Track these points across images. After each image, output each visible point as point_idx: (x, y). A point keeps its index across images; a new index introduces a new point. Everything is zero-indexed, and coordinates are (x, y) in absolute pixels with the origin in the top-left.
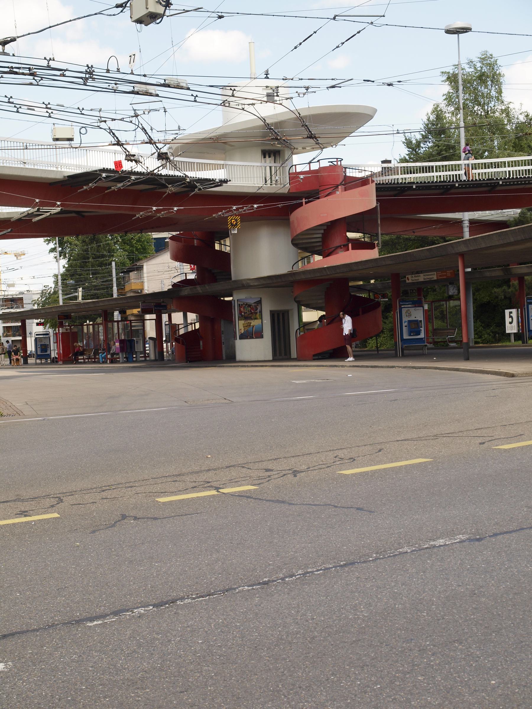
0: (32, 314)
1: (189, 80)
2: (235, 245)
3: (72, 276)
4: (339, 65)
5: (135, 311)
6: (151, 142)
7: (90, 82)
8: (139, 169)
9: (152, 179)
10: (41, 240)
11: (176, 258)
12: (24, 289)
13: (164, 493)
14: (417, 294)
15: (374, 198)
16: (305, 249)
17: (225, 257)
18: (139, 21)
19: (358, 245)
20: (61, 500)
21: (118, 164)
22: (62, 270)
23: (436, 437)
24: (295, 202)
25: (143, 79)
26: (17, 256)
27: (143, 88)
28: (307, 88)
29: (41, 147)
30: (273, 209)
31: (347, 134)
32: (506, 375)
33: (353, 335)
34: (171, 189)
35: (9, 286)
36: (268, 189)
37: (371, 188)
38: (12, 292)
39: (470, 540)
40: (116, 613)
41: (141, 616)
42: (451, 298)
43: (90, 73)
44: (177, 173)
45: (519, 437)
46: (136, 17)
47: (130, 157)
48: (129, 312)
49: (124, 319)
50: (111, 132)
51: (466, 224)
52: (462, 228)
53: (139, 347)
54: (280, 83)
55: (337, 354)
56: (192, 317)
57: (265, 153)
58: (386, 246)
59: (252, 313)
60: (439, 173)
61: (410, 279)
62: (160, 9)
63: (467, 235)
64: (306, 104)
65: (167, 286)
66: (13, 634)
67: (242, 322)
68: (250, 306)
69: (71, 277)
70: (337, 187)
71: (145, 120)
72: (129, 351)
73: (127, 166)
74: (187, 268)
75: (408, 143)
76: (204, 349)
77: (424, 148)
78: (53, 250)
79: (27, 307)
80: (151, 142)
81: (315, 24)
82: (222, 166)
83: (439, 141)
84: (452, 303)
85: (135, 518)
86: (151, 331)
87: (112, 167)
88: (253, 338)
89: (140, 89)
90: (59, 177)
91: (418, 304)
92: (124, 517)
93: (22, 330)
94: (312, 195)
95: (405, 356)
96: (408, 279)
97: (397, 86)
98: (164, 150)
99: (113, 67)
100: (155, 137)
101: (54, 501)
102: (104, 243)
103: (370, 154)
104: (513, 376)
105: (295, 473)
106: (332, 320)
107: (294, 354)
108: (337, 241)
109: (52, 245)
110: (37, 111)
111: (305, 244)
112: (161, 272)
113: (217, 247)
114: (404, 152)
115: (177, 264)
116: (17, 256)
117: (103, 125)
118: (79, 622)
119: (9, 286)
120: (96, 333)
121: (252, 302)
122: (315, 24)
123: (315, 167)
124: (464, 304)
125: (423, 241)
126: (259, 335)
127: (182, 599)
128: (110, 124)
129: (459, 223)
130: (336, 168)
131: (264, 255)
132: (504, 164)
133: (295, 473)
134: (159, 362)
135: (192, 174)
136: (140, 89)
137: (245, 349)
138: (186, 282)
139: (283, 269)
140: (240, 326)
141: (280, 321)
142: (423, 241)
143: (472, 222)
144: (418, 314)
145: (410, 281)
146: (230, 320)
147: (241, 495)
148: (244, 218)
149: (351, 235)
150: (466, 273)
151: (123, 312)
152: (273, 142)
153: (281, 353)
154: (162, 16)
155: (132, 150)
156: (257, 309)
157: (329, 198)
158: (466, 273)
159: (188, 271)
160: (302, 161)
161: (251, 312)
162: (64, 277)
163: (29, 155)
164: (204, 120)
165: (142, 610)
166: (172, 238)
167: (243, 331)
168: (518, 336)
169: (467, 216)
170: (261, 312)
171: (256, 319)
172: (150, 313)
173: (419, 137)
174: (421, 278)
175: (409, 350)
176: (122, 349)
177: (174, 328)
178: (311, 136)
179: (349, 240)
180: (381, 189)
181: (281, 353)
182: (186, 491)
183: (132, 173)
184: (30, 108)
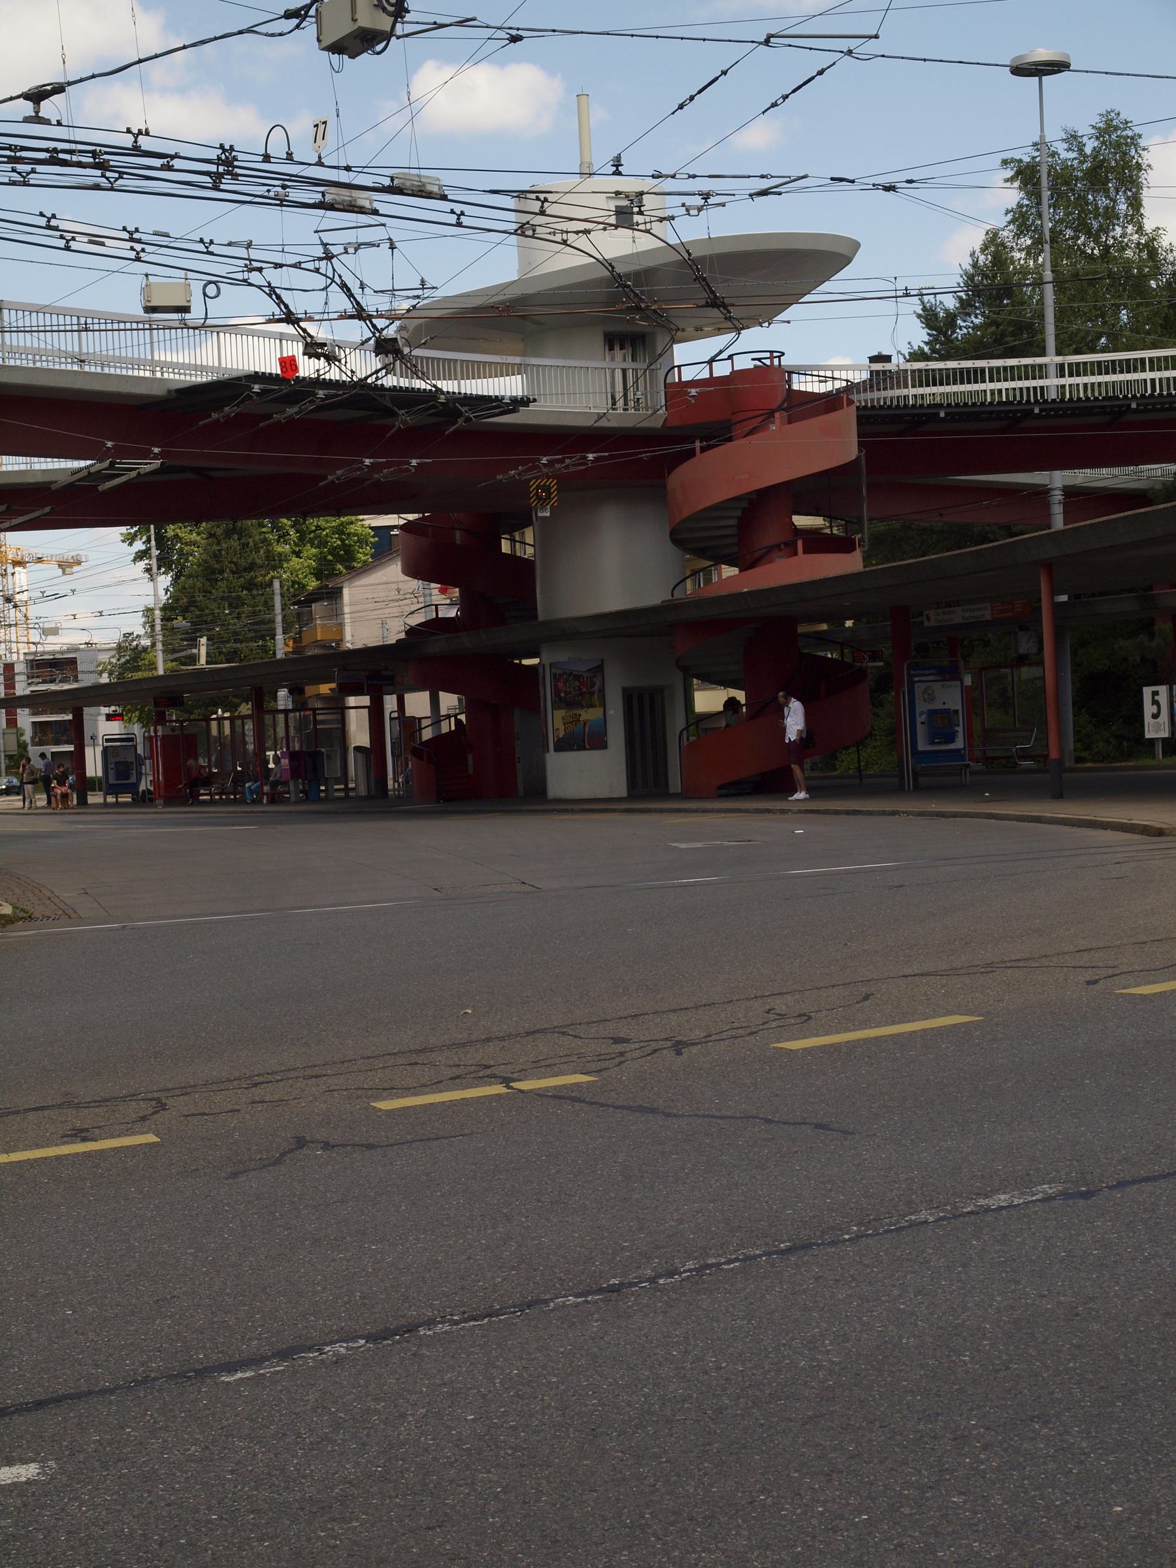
0: (98, 695)
1: (446, 178)
2: (543, 544)
3: (184, 611)
4: (760, 143)
5: (325, 689)
6: (360, 314)
7: (227, 183)
8: (334, 374)
9: (361, 394)
10: (115, 533)
11: (413, 570)
13: (390, 1091)
14: (948, 653)
16: (701, 553)
18: (337, 48)
19: (816, 542)
21: (288, 363)
22: (163, 598)
23: (990, 967)
24: (678, 448)
25: (344, 177)
26: (65, 565)
27: (344, 195)
28: (706, 196)
30: (629, 462)
31: (794, 298)
32: (1145, 830)
34: (404, 418)
35: (46, 632)
36: (622, 418)
37: (848, 418)
38: (53, 645)
40: (283, 1355)
41: (339, 1360)
42: (1022, 660)
43: (225, 164)
46: (329, 40)
47: (313, 349)
48: (310, 690)
49: (300, 703)
51: (1058, 496)
52: (1047, 506)
53: (331, 769)
54: (648, 184)
55: (771, 783)
56: (449, 701)
57: (613, 341)
58: (879, 547)
59: (582, 694)
60: (996, 383)
61: (934, 618)
63: (1058, 522)
64: (692, 230)
65: (394, 634)
66: (57, 1400)
67: (560, 714)
68: (577, 677)
69: (181, 614)
70: (771, 414)
71: (348, 267)
72: (310, 779)
73: (308, 368)
75: (929, 317)
76: (477, 774)
77: (964, 328)
78: (140, 556)
79: (86, 681)
80: (360, 314)
81: (724, 55)
84: (1026, 672)
85: (326, 1146)
86: (359, 732)
87: (276, 369)
88: (583, 748)
89: (340, 198)
91: (950, 673)
92: (301, 1143)
93: (76, 732)
94: (717, 433)
95: (920, 789)
96: (928, 618)
98: (391, 332)
99: (277, 149)
100: (371, 303)
101: (146, 1108)
103: (830, 343)
104: (1160, 833)
105: (678, 1047)
108: (771, 535)
109: (139, 545)
111: (698, 540)
112: (382, 604)
113: (505, 547)
114: (919, 336)
115: (415, 584)
116: (65, 565)
117: (255, 277)
118: (203, 1373)
119: (46, 632)
120: (238, 738)
121: (582, 668)
122: (724, 55)
123: (722, 369)
124: (1053, 673)
125: (963, 535)
126: (598, 741)
127: (430, 1323)
129: (1041, 494)
130: (769, 375)
131: (614, 567)
132: (1155, 364)
133: (678, 1047)
134: (376, 802)
135: (448, 386)
136: (340, 198)
137: (579, 773)
138: (436, 625)
139: (652, 595)
140: (556, 721)
141: (646, 713)
142: (963, 535)
143: (1070, 492)
144: (950, 697)
145: (933, 623)
147: (559, 1096)
148: (566, 483)
149: (800, 521)
151: (296, 691)
152: (630, 311)
153: (647, 784)
154: (387, 36)
155: (318, 331)
156: (593, 686)
157: (754, 439)
159: (444, 603)
160: (694, 357)
161: (581, 690)
163: (92, 344)
164: (480, 265)
166: (407, 527)
167: (562, 734)
169: (1059, 479)
170: (602, 691)
171: (592, 706)
172: (358, 692)
173: (950, 303)
174: (958, 616)
176: (295, 772)
177: (409, 725)
178: (714, 303)
180: (869, 418)
181: (647, 784)
182: (437, 1085)
183: (317, 383)
184: (95, 240)
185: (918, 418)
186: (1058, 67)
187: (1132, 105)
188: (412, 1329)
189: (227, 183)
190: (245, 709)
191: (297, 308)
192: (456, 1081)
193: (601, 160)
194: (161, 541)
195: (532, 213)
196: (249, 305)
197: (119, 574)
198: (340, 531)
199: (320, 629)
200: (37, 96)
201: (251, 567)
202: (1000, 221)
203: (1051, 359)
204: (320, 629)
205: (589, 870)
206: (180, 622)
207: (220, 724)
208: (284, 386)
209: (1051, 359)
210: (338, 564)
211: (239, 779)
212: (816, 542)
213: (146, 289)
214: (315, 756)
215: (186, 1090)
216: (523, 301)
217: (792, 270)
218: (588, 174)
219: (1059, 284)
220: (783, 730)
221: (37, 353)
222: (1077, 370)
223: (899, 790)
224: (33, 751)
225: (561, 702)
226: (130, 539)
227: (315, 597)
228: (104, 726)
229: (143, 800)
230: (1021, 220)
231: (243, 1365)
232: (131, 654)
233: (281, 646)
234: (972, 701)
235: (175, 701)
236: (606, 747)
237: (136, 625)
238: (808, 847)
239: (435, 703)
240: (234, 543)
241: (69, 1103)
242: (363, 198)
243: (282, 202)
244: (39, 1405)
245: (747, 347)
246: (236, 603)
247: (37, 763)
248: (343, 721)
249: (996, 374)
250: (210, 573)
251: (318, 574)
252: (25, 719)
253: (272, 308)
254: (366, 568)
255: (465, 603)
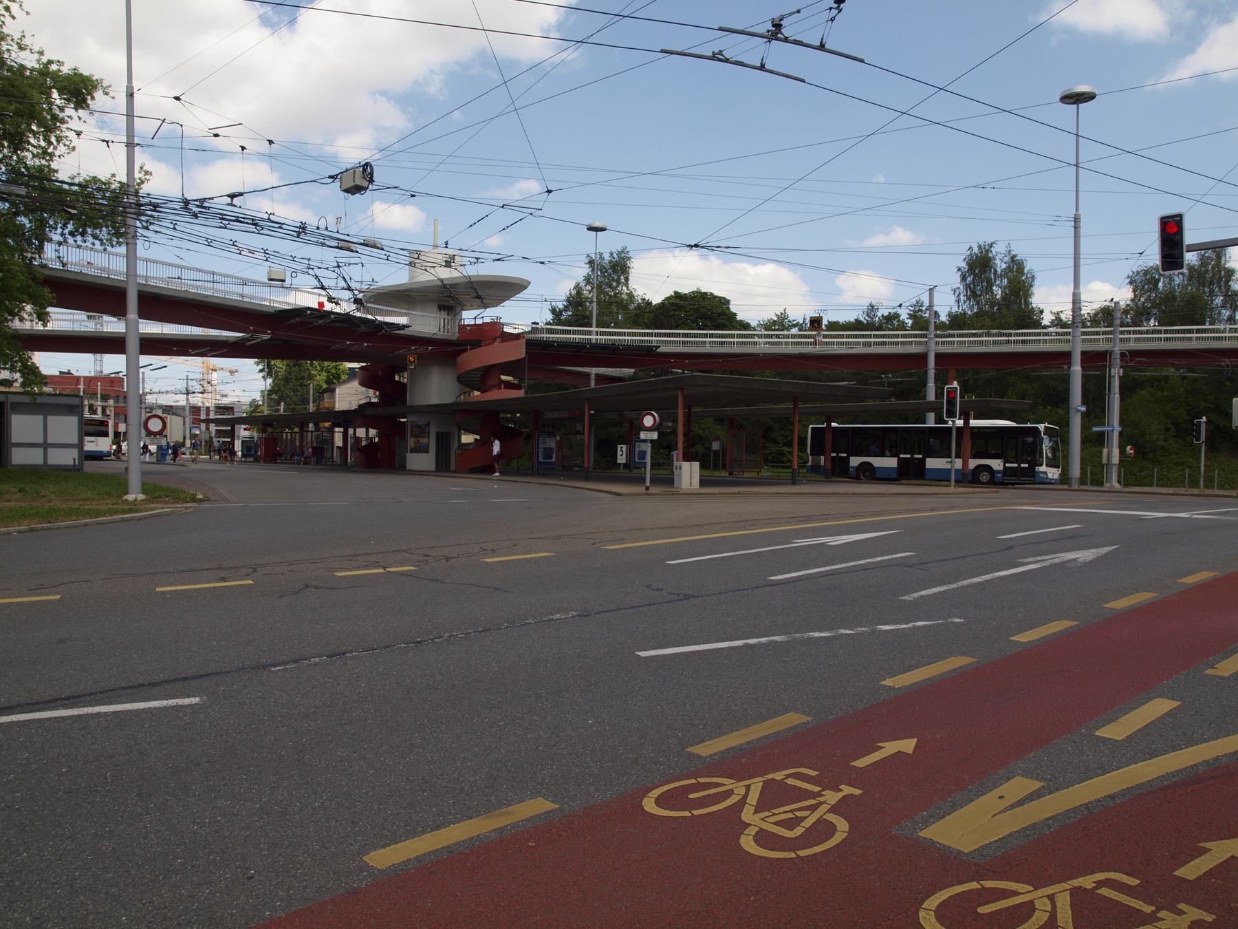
0: (241, 421)
1: (384, 243)
2: (411, 378)
3: (276, 393)
4: (495, 243)
5: (327, 424)
6: (349, 289)
7: (302, 236)
8: (337, 309)
9: (347, 318)
10: (252, 361)
11: (362, 384)
12: (236, 399)
13: (342, 569)
14: (552, 428)
15: (524, 350)
16: (467, 386)
17: (402, 387)
18: (347, 191)
19: (508, 385)
20: (255, 570)
21: (321, 304)
22: (269, 387)
23: (559, 537)
24: (457, 348)
25: (346, 238)
26: (232, 372)
27: (346, 245)
28: (477, 259)
29: (262, 284)
30: (444, 351)
31: (508, 298)
32: (615, 494)
33: (500, 455)
34: (363, 328)
35: (223, 396)
36: (442, 335)
37: (523, 342)
38: (225, 401)
39: (579, 616)
40: (295, 661)
41: (316, 664)
42: (577, 432)
43: (303, 228)
44: (370, 317)
45: (621, 541)
46: (345, 187)
47: (331, 299)
48: (321, 425)
49: (317, 430)
50: (317, 277)
51: (593, 377)
52: (589, 379)
53: (328, 454)
54: (457, 252)
55: (487, 469)
56: (373, 432)
57: (441, 308)
58: (530, 389)
60: (574, 336)
61: (548, 415)
62: (365, 184)
63: (593, 385)
64: (472, 271)
65: (354, 406)
66: (208, 675)
69: (274, 395)
70: (495, 339)
71: (345, 271)
72: (320, 457)
73: (328, 307)
74: (371, 392)
75: (553, 311)
76: (380, 459)
77: (565, 316)
78: (261, 371)
79: (237, 415)
80: (349, 289)
81: (488, 210)
82: (406, 315)
83: (575, 310)
84: (578, 437)
85: (316, 588)
86: (338, 441)
87: (316, 307)
89: (345, 245)
90: (271, 310)
91: (552, 435)
92: (307, 586)
93: (232, 434)
94: (476, 344)
95: (539, 475)
97: (547, 264)
98: (360, 296)
99: (322, 226)
100: (353, 285)
101: (249, 571)
102: (86, 402)
103: (519, 316)
104: (620, 495)
105: (447, 559)
106: (485, 444)
107: (453, 467)
108: (492, 381)
109: (261, 367)
110: (257, 255)
111: (466, 381)
112: (349, 396)
113: (397, 378)
114: (550, 317)
115: (363, 389)
116: (232, 372)
117: (310, 271)
118: (264, 667)
119: (223, 396)
120: (293, 440)
122: (488, 210)
123: (479, 322)
124: (587, 438)
125: (560, 387)
126: (425, 450)
127: (351, 652)
128: (318, 272)
129: (588, 375)
130: (496, 326)
131: (435, 388)
132: (629, 334)
133: (447, 559)
134: (344, 467)
135: (380, 318)
136: (345, 245)
137: (417, 461)
138: (370, 404)
139: (449, 399)
140: (411, 442)
141: (444, 441)
142: (560, 387)
143: (597, 375)
144: (552, 443)
146: (404, 437)
147: (403, 574)
148: (420, 357)
149: (503, 378)
150: (590, 415)
151: (316, 425)
152: (448, 298)
153: (442, 466)
154: (366, 189)
155: (333, 294)
158: (590, 415)
159: (373, 396)
160: (469, 317)
161: (421, 432)
162: (270, 392)
163: (248, 290)
164: (394, 276)
165: (317, 660)
166: (361, 368)
168: (626, 466)
169: (594, 371)
172: (339, 426)
173: (561, 306)
174: (556, 415)
175: (543, 470)
176: (314, 454)
177: (357, 440)
178: (478, 297)
179: (502, 381)
180: (529, 343)
181: (442, 466)
182: (359, 568)
183: (331, 313)
184: (251, 252)
185: (547, 345)
186: (603, 229)
187: (631, 244)
188: (344, 654)
189: (302, 236)
190: (297, 430)
191: (326, 283)
192: (366, 567)
193: (441, 242)
194: (269, 366)
195: (414, 259)
196: (308, 281)
197: (251, 377)
198: (336, 367)
199: (326, 403)
200: (232, 196)
201: (303, 378)
202: (581, 279)
203: (594, 329)
204: (326, 403)
205: (419, 494)
206: (274, 396)
207: (287, 434)
208: (319, 313)
209: (594, 329)
210: (334, 380)
211: (293, 455)
212: (508, 385)
213: (269, 272)
214: (322, 449)
215: (264, 566)
216: (410, 290)
217: (506, 289)
218: (436, 246)
219: (598, 303)
220: (502, 447)
221: (225, 292)
222: (602, 334)
223: (531, 474)
224: (215, 440)
225: (413, 435)
226: (258, 364)
227: (325, 391)
228: (243, 432)
229: (257, 460)
230: (588, 280)
231: (280, 664)
232: (254, 405)
233: (312, 408)
234: (559, 444)
235: (271, 425)
236: (1180, 216)
237: (257, 396)
238: (497, 491)
239: (367, 432)
240: (296, 369)
241: (220, 568)
242: (353, 247)
243: (323, 245)
244: (201, 676)
245: (486, 315)
246: (296, 391)
247: (216, 444)
248: (333, 437)
249: (575, 332)
250: (287, 380)
251: (327, 382)
252: (213, 428)
253: (316, 283)
254: (345, 382)
255: (380, 397)
